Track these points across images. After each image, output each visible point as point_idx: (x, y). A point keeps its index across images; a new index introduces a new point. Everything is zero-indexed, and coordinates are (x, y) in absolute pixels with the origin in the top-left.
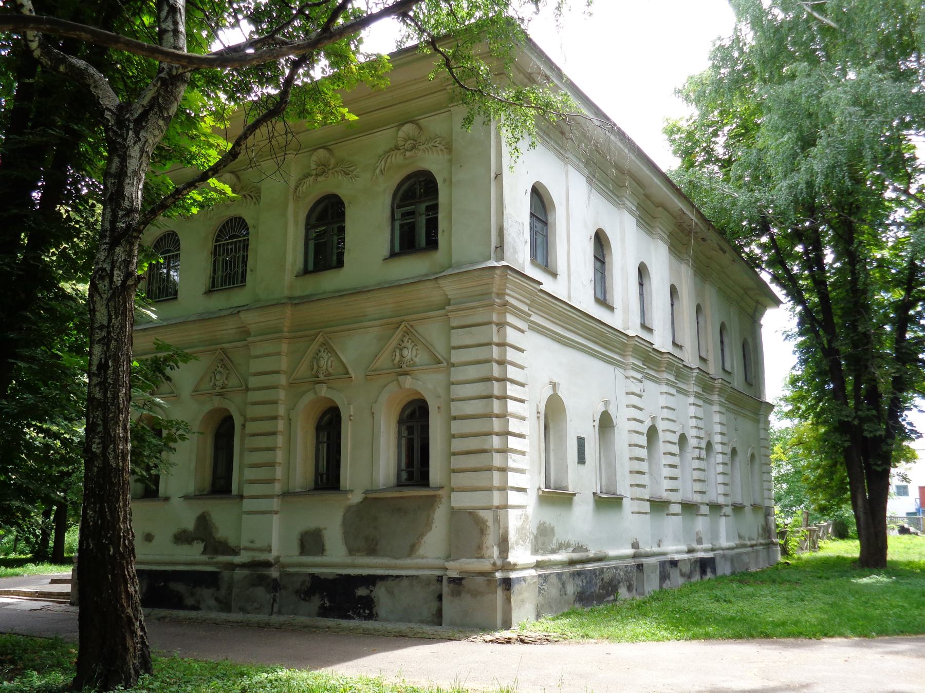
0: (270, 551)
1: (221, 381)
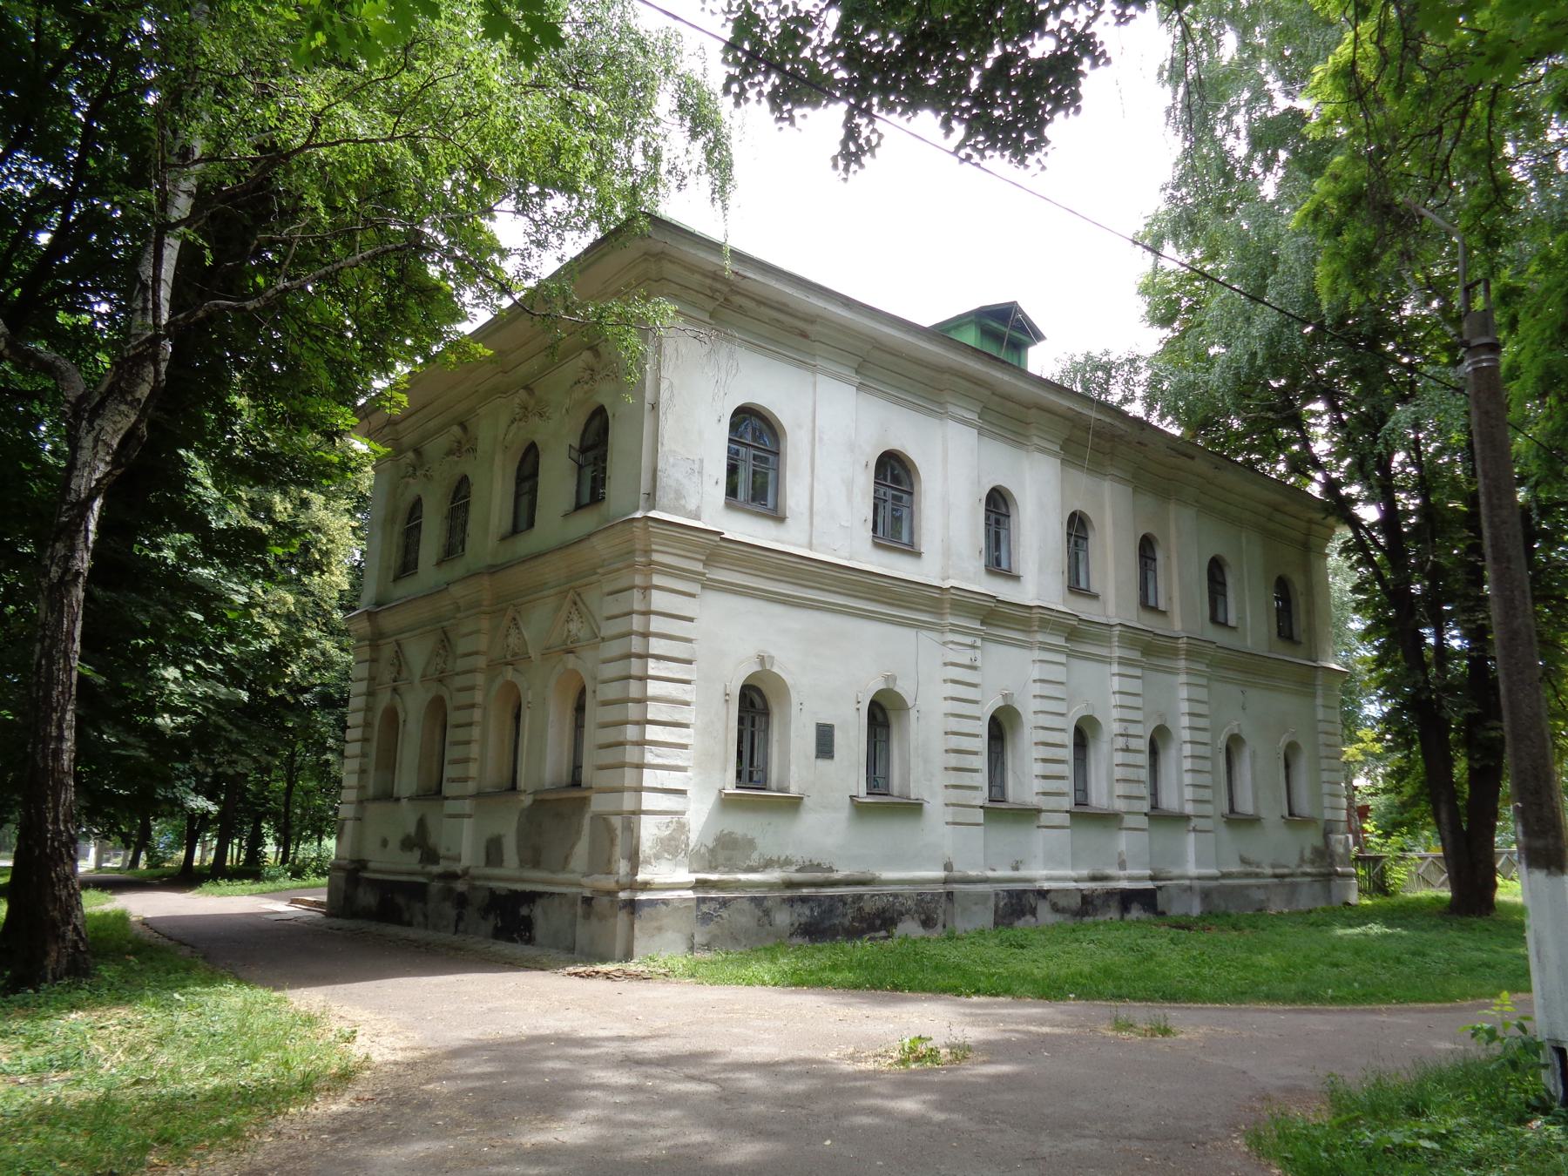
0: (460, 860)
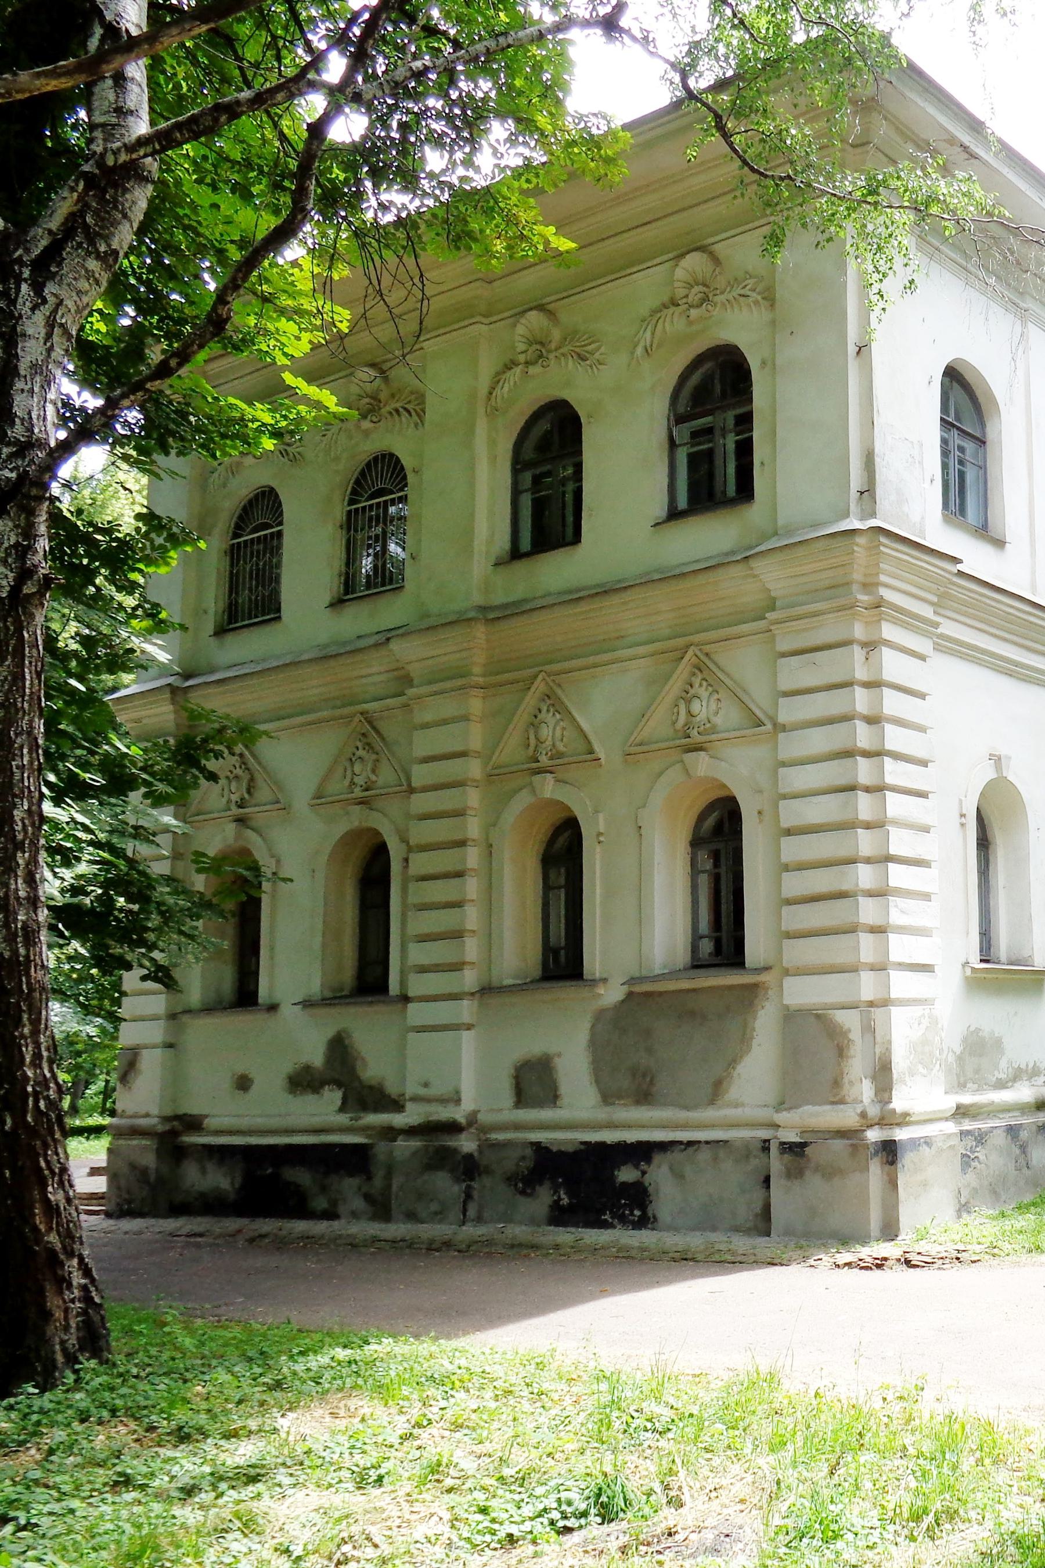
0: (458, 1101)
1: (364, 774)
